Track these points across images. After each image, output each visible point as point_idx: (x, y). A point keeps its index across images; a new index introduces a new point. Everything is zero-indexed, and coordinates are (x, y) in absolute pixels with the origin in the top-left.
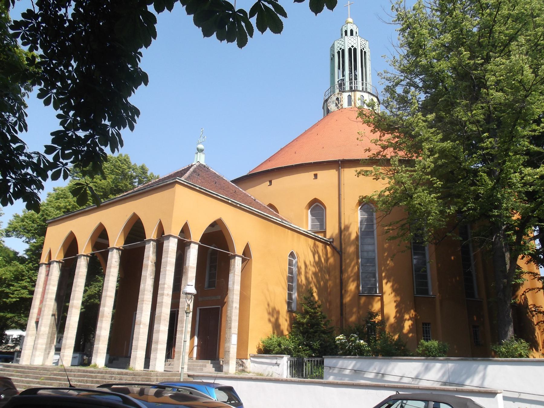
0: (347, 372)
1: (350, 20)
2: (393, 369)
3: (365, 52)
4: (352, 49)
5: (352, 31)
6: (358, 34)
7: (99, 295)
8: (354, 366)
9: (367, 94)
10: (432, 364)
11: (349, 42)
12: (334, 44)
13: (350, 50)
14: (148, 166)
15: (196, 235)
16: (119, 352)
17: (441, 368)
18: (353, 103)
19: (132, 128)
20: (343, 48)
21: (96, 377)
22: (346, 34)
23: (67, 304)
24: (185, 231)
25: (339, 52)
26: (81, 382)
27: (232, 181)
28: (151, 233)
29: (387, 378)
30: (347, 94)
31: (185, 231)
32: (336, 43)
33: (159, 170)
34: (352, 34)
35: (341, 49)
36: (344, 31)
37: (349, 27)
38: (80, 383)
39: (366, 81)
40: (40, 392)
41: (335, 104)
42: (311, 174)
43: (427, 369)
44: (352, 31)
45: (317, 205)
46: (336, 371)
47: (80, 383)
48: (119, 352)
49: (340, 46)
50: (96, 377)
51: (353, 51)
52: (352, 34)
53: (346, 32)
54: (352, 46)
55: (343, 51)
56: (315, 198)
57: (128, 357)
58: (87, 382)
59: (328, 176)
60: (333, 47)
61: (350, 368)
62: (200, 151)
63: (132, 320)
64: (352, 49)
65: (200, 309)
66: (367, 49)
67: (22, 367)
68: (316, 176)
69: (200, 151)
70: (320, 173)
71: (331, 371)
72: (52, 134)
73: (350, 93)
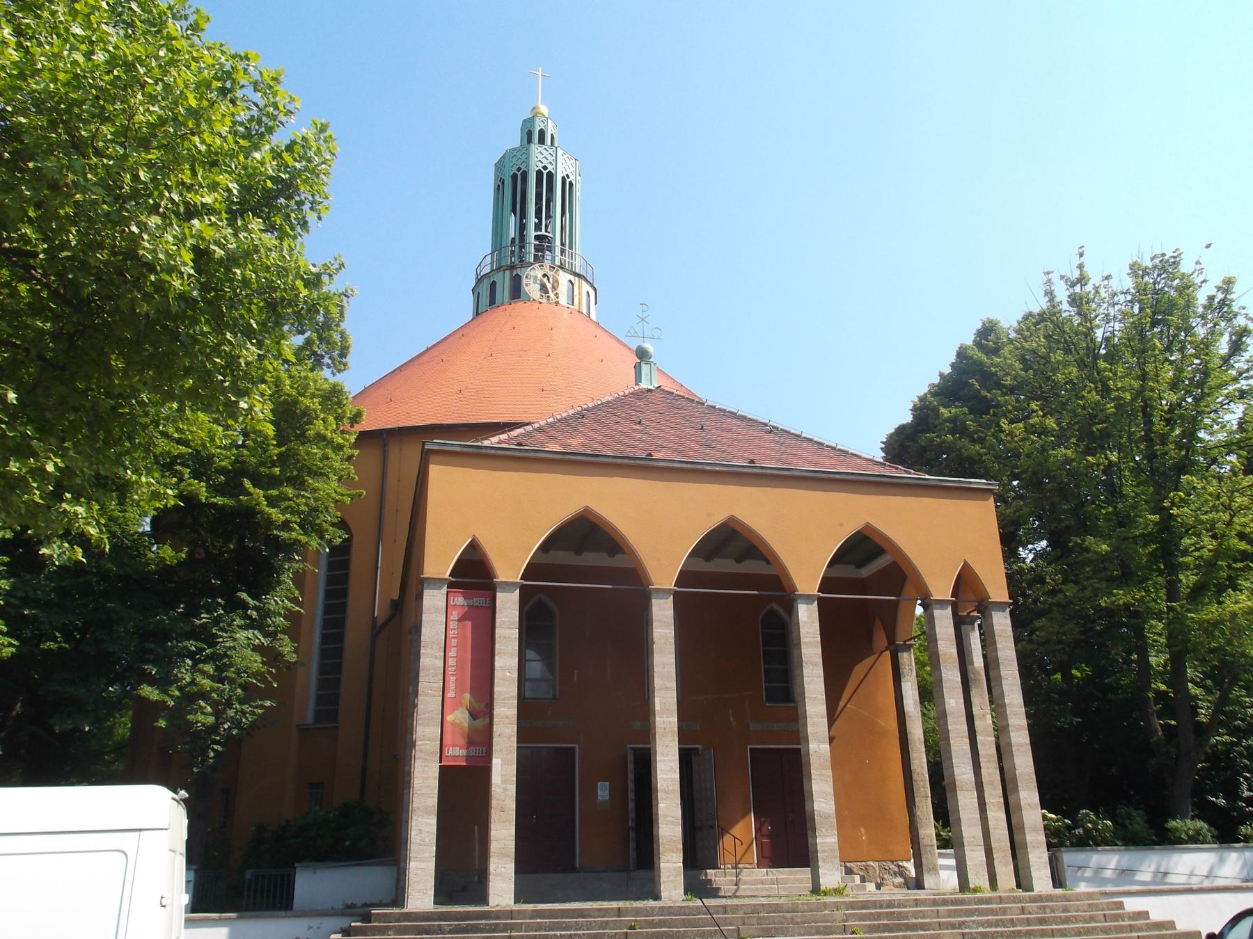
0: (1108, 874)
2: (1176, 865)
4: (545, 172)
5: (542, 133)
7: (943, 715)
8: (1118, 862)
10: (1226, 854)
13: (539, 173)
17: (1238, 859)
20: (550, 168)
21: (1004, 911)
24: (966, 582)
25: (514, 177)
26: (997, 926)
29: (1172, 879)
31: (966, 582)
34: (542, 141)
35: (519, 169)
38: (994, 929)
39: (571, 248)
41: (538, 287)
43: (1222, 861)
46: (1088, 874)
47: (994, 929)
49: (545, 162)
50: (1004, 911)
54: (545, 168)
55: (525, 175)
58: (990, 924)
61: (1112, 865)
63: (801, 771)
64: (545, 172)
65: (573, 749)
67: (498, 914)
71: (1079, 874)
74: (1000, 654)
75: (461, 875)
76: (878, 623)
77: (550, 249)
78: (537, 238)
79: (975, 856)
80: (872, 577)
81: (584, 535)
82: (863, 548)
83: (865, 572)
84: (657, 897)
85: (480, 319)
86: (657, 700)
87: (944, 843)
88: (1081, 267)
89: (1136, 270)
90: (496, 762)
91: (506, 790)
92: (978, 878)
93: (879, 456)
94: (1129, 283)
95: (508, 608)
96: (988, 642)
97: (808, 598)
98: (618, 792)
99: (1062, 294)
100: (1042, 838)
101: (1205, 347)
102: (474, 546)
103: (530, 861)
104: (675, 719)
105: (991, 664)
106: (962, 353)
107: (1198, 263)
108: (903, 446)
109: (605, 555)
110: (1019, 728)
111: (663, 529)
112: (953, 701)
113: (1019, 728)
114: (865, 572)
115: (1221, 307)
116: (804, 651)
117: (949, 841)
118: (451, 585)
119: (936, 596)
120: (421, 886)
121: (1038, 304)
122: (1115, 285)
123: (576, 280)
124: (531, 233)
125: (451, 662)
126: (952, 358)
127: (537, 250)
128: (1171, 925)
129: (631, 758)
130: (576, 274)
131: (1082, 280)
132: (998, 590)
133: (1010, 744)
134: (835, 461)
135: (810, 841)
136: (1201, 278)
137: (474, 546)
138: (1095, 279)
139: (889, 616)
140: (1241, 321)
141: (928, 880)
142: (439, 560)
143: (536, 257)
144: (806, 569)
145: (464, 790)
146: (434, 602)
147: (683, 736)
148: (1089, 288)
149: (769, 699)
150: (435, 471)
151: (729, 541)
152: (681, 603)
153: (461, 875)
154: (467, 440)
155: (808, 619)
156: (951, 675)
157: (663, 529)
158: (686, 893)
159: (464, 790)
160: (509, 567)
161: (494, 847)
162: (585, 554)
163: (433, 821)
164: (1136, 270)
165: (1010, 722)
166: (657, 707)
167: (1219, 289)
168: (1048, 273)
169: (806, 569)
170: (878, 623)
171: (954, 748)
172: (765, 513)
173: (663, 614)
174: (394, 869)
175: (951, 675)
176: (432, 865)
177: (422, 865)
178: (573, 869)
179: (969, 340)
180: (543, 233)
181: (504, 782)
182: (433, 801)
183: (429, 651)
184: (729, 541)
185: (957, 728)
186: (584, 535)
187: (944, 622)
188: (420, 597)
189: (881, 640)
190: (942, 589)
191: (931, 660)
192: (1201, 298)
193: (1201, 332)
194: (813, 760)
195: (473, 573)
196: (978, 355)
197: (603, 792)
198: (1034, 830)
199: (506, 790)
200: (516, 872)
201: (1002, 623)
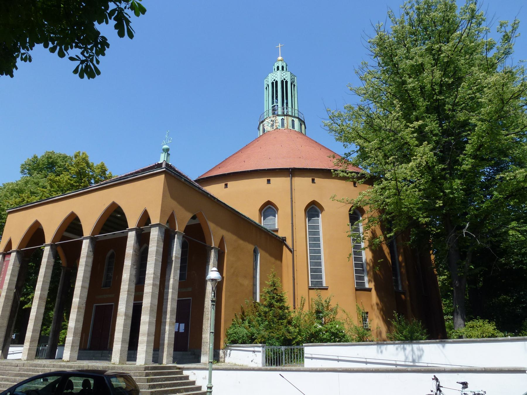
9: (297, 120)
13: (282, 82)
14: (107, 166)
15: (179, 228)
16: (96, 339)
18: (286, 125)
24: (145, 219)
27: (196, 181)
28: (133, 222)
30: (281, 118)
31: (145, 219)
33: (116, 171)
40: (18, 390)
42: (265, 180)
44: (283, 67)
45: (270, 207)
48: (96, 339)
52: (283, 69)
54: (284, 79)
55: (277, 82)
56: (314, 201)
57: (111, 350)
59: (280, 183)
68: (269, 181)
70: (273, 180)
72: (89, 79)
73: (283, 117)
157: (89, 209)
190: (133, 222)
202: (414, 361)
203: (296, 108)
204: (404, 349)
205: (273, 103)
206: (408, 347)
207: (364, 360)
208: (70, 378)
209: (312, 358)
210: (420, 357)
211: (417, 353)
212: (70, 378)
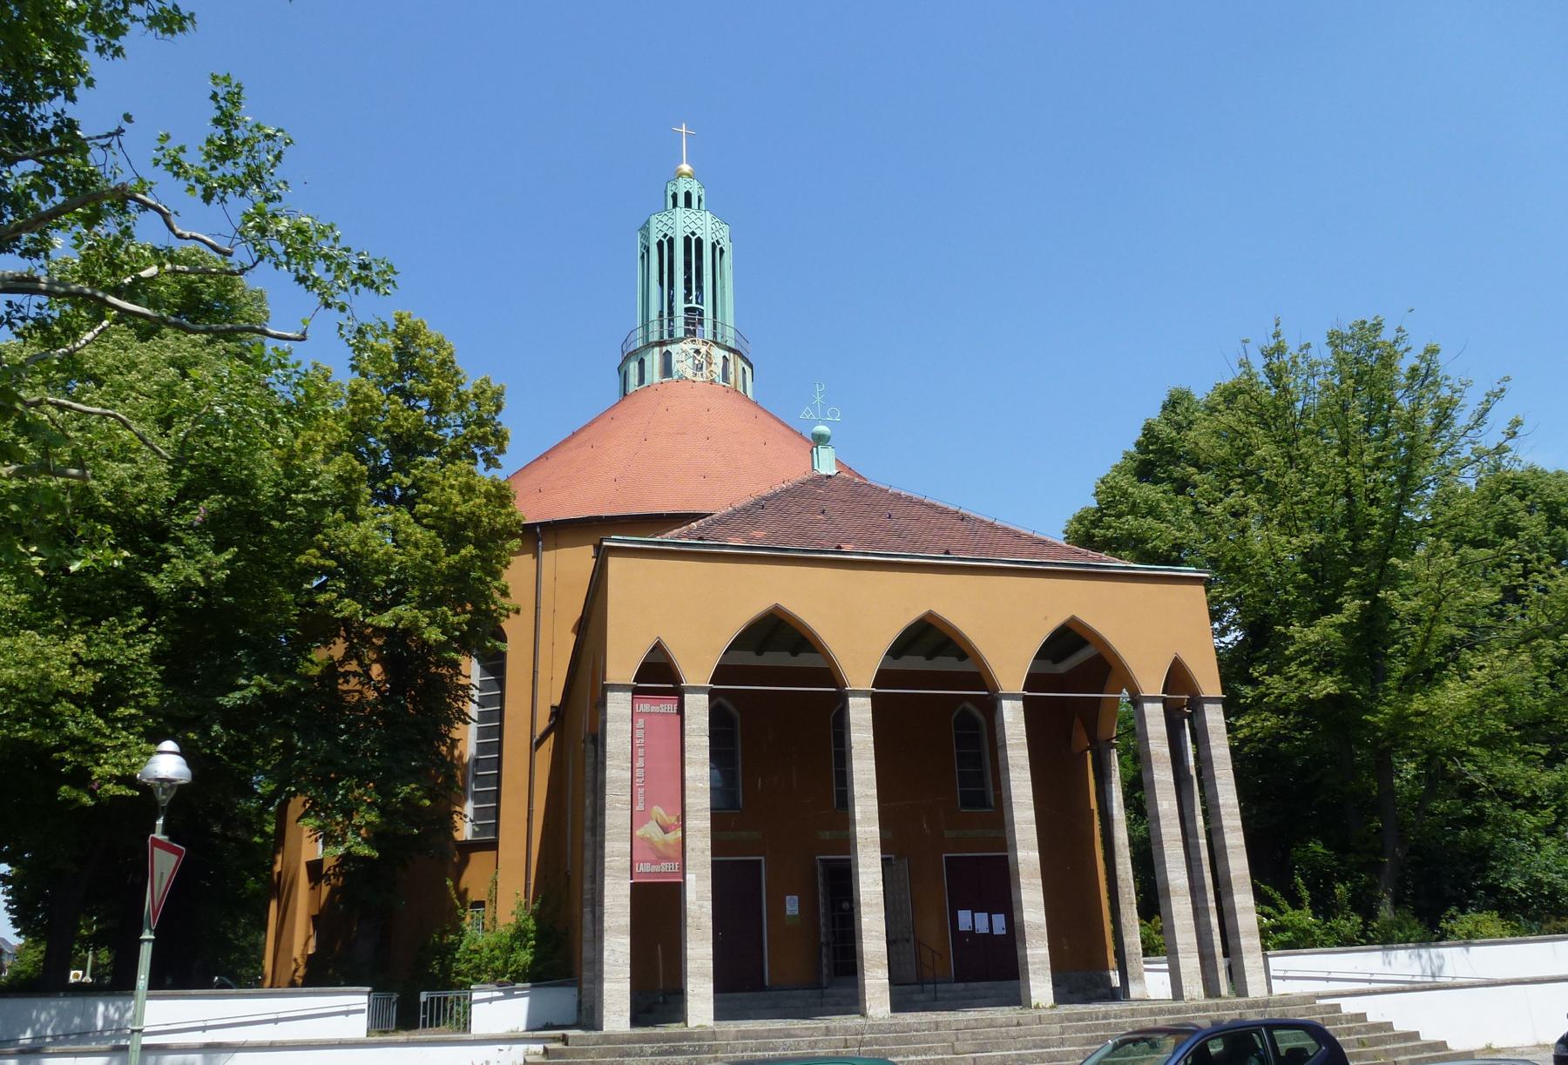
1: (686, 168)
3: (722, 251)
5: (688, 196)
6: (703, 206)
11: (681, 223)
12: (648, 222)
13: (687, 240)
19: (1377, 327)
20: (670, 233)
22: (675, 205)
23: (169, 981)
24: (1178, 677)
25: (660, 244)
31: (1178, 677)
32: (653, 220)
34: (688, 204)
36: (670, 193)
37: (682, 187)
44: (688, 196)
51: (693, 246)
52: (688, 204)
53: (675, 197)
54: (693, 234)
55: (671, 242)
60: (645, 229)
62: (820, 439)
66: (726, 244)
69: (820, 439)
74: (1213, 752)
75: (657, 996)
76: (1077, 721)
77: (701, 323)
78: (687, 310)
79: (1190, 963)
80: (1070, 672)
81: (775, 633)
82: (1068, 641)
83: (1062, 668)
84: (863, 1015)
85: (628, 401)
86: (857, 809)
87: (1149, 950)
88: (1277, 335)
89: (1335, 339)
90: (691, 878)
91: (701, 907)
92: (1193, 987)
93: (1058, 538)
94: (1327, 353)
95: (698, 708)
96: (1200, 738)
97: (1153, 699)
98: (809, 907)
99: (1258, 364)
100: (1257, 942)
101: (1411, 424)
102: (658, 648)
103: (723, 984)
104: (876, 829)
105: (1204, 761)
106: (1149, 431)
107: (1399, 330)
108: (1086, 534)
109: (752, 654)
110: (1233, 830)
111: (856, 622)
112: (1166, 804)
113: (1233, 830)
114: (1062, 668)
115: (1423, 377)
116: (1009, 753)
117: (1158, 946)
118: (636, 692)
119: (1146, 692)
120: (616, 1008)
121: (1229, 376)
122: (1314, 355)
123: (731, 356)
124: (680, 305)
125: (639, 773)
126: (1138, 435)
127: (687, 323)
128: (1415, 1036)
129: (820, 870)
130: (730, 350)
131: (1279, 350)
132: (1209, 682)
133: (1224, 847)
134: (1033, 549)
135: (1020, 953)
136: (1403, 347)
137: (658, 648)
138: (1292, 349)
139: (1091, 714)
140: (1445, 393)
141: (1135, 990)
142: (622, 664)
143: (687, 331)
144: (1010, 666)
145: (657, 908)
146: (618, 706)
147: (886, 846)
148: (1286, 358)
149: (965, 804)
150: (614, 563)
151: (928, 638)
152: (879, 704)
153: (657, 996)
154: (649, 531)
155: (1013, 716)
156: (1163, 776)
157: (856, 622)
158: (893, 1010)
159: (657, 908)
160: (697, 669)
161: (691, 966)
162: (905, 658)
163: (627, 940)
164: (1335, 339)
165: (1225, 823)
166: (858, 817)
167: (1422, 359)
168: (1245, 341)
169: (1010, 666)
170: (1077, 721)
171: (1167, 852)
172: (965, 605)
173: (860, 713)
174: (575, 991)
175: (1163, 776)
176: (626, 986)
177: (617, 986)
178: (759, 986)
179: (1154, 413)
180: (694, 305)
181: (700, 898)
182: (625, 920)
183: (615, 762)
184: (928, 638)
185: (1170, 830)
186: (775, 633)
187: (1155, 717)
188: (603, 703)
189: (1081, 739)
190: (1151, 682)
191: (1139, 760)
192: (1404, 364)
193: (1405, 403)
194: (1022, 868)
195: (658, 674)
196: (1167, 432)
197: (792, 906)
198: (1250, 934)
199: (701, 907)
200: (716, 990)
201: (1214, 717)
202: (1433, 976)
203: (730, 320)
204: (1420, 956)
205: (687, 299)
206: (1423, 952)
207: (1324, 975)
208: (1283, 1053)
209: (1284, 978)
210: (1441, 968)
211: (1436, 962)
212: (1283, 1053)
